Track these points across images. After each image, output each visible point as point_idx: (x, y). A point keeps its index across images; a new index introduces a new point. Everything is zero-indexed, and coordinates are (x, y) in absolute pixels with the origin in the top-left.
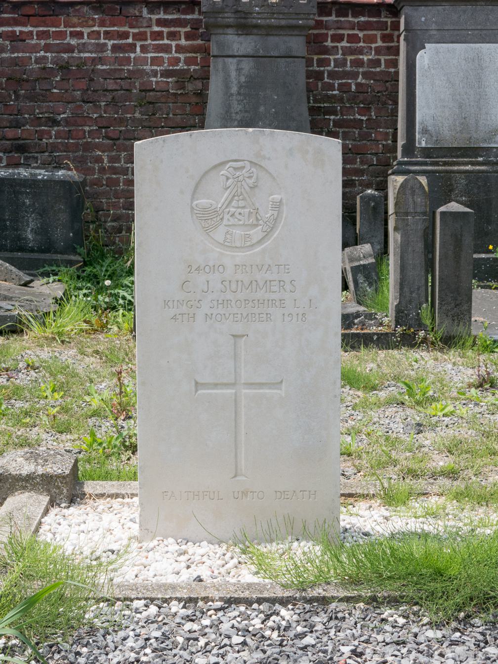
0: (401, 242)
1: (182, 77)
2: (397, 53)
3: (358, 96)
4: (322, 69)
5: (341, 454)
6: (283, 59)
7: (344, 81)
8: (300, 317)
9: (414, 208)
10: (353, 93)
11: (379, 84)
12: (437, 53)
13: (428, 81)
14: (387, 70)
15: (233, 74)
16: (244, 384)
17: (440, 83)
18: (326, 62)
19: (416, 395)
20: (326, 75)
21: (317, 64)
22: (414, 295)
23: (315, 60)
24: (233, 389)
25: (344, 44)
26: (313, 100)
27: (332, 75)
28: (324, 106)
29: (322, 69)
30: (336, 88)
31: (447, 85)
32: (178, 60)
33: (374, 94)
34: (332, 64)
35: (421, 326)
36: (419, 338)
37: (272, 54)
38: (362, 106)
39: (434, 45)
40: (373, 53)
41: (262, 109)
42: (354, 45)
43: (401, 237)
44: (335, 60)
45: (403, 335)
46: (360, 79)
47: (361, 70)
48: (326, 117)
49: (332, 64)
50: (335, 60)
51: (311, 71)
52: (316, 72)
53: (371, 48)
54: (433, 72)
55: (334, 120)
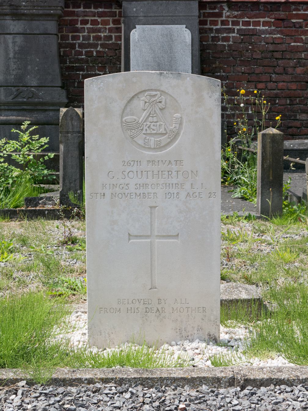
0: (64, 151)
3: (98, 59)
4: (75, 42)
6: (42, 35)
7: (89, 49)
8: (175, 195)
9: (73, 129)
10: (95, 57)
11: (111, 51)
12: (144, 31)
13: (138, 49)
14: (116, 42)
16: (157, 236)
17: (146, 50)
18: (78, 38)
20: (77, 46)
21: (71, 38)
22: (72, 185)
23: (70, 36)
24: (149, 239)
25: (89, 26)
26: (69, 62)
27: (81, 46)
28: (76, 66)
29: (75, 42)
30: (84, 54)
31: (150, 51)
33: (108, 58)
34: (81, 39)
36: (74, 213)
37: (35, 32)
38: (100, 65)
39: (141, 26)
40: (107, 31)
41: (29, 67)
42: (95, 26)
43: (64, 147)
44: (83, 36)
45: (64, 211)
47: (99, 42)
48: (77, 72)
49: (81, 39)
50: (83, 36)
51: (68, 43)
52: (71, 44)
53: (106, 28)
54: (141, 43)
55: (82, 75)
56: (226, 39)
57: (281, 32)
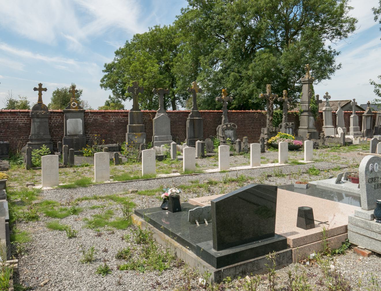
1: (26, 124)
2: (64, 119)
5: (60, 167)
15: (36, 125)
19: (66, 174)
32: (25, 121)
35: (67, 165)
46: (57, 124)
56: (90, 121)
57: (103, 119)
